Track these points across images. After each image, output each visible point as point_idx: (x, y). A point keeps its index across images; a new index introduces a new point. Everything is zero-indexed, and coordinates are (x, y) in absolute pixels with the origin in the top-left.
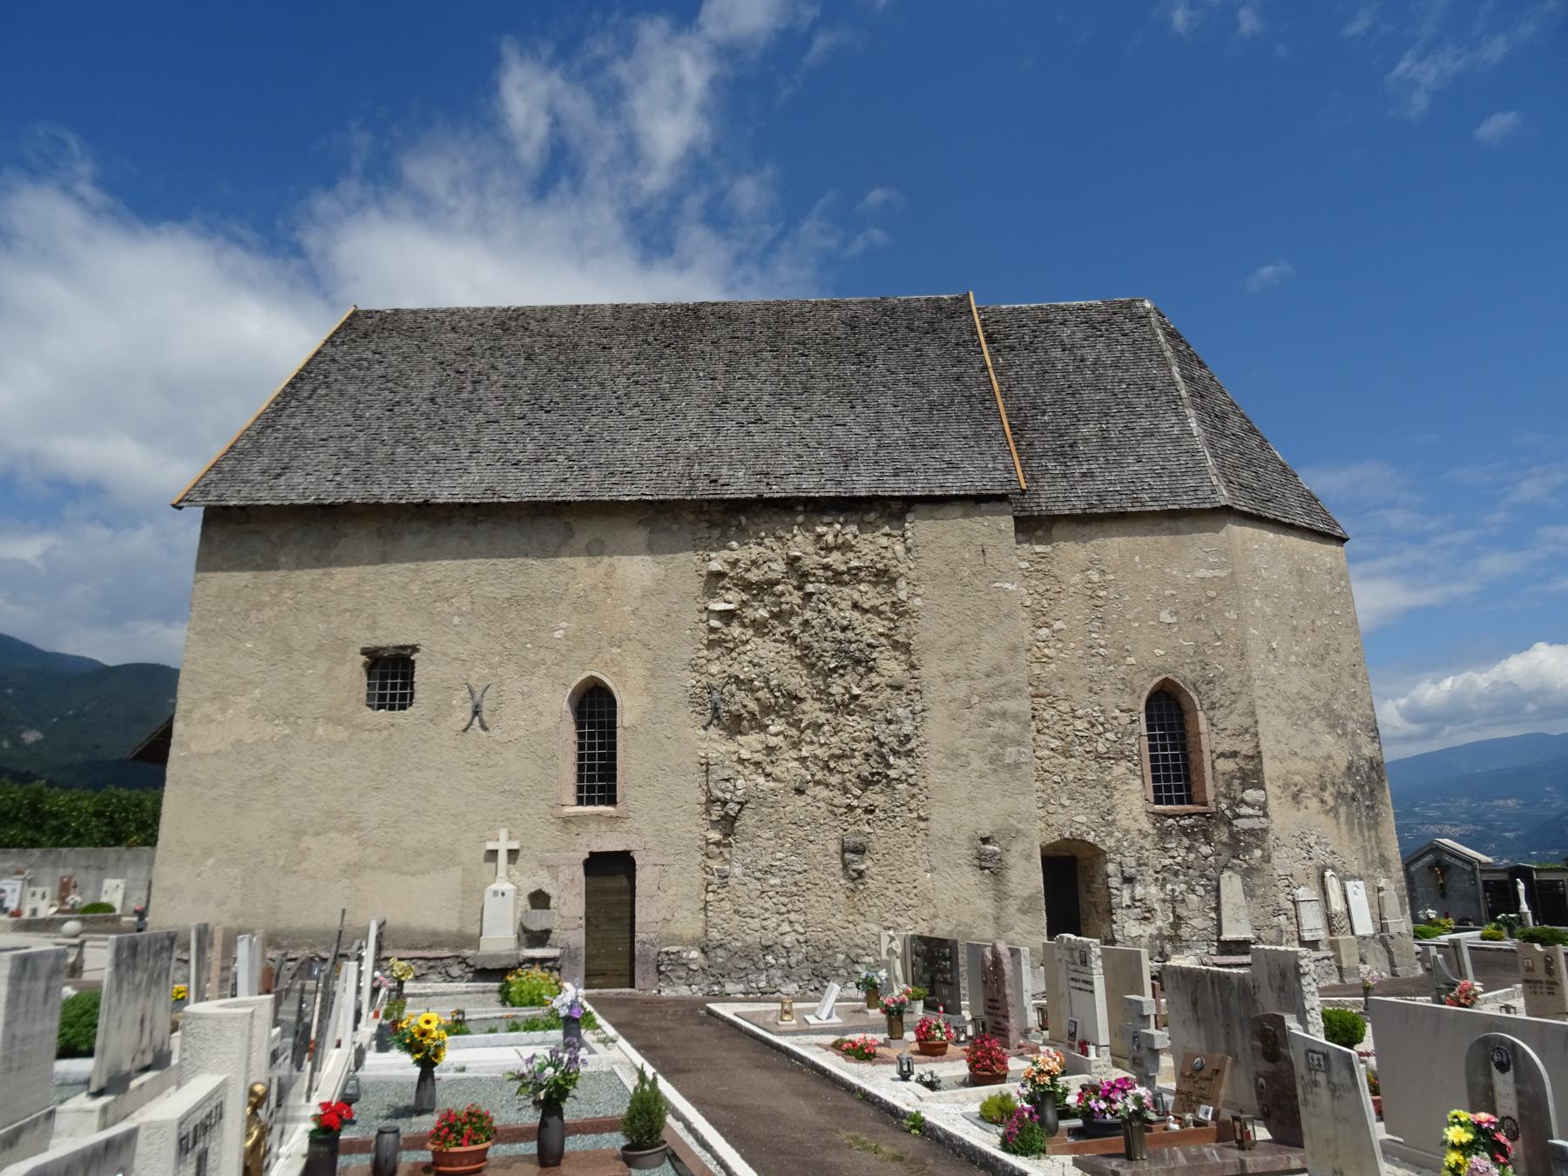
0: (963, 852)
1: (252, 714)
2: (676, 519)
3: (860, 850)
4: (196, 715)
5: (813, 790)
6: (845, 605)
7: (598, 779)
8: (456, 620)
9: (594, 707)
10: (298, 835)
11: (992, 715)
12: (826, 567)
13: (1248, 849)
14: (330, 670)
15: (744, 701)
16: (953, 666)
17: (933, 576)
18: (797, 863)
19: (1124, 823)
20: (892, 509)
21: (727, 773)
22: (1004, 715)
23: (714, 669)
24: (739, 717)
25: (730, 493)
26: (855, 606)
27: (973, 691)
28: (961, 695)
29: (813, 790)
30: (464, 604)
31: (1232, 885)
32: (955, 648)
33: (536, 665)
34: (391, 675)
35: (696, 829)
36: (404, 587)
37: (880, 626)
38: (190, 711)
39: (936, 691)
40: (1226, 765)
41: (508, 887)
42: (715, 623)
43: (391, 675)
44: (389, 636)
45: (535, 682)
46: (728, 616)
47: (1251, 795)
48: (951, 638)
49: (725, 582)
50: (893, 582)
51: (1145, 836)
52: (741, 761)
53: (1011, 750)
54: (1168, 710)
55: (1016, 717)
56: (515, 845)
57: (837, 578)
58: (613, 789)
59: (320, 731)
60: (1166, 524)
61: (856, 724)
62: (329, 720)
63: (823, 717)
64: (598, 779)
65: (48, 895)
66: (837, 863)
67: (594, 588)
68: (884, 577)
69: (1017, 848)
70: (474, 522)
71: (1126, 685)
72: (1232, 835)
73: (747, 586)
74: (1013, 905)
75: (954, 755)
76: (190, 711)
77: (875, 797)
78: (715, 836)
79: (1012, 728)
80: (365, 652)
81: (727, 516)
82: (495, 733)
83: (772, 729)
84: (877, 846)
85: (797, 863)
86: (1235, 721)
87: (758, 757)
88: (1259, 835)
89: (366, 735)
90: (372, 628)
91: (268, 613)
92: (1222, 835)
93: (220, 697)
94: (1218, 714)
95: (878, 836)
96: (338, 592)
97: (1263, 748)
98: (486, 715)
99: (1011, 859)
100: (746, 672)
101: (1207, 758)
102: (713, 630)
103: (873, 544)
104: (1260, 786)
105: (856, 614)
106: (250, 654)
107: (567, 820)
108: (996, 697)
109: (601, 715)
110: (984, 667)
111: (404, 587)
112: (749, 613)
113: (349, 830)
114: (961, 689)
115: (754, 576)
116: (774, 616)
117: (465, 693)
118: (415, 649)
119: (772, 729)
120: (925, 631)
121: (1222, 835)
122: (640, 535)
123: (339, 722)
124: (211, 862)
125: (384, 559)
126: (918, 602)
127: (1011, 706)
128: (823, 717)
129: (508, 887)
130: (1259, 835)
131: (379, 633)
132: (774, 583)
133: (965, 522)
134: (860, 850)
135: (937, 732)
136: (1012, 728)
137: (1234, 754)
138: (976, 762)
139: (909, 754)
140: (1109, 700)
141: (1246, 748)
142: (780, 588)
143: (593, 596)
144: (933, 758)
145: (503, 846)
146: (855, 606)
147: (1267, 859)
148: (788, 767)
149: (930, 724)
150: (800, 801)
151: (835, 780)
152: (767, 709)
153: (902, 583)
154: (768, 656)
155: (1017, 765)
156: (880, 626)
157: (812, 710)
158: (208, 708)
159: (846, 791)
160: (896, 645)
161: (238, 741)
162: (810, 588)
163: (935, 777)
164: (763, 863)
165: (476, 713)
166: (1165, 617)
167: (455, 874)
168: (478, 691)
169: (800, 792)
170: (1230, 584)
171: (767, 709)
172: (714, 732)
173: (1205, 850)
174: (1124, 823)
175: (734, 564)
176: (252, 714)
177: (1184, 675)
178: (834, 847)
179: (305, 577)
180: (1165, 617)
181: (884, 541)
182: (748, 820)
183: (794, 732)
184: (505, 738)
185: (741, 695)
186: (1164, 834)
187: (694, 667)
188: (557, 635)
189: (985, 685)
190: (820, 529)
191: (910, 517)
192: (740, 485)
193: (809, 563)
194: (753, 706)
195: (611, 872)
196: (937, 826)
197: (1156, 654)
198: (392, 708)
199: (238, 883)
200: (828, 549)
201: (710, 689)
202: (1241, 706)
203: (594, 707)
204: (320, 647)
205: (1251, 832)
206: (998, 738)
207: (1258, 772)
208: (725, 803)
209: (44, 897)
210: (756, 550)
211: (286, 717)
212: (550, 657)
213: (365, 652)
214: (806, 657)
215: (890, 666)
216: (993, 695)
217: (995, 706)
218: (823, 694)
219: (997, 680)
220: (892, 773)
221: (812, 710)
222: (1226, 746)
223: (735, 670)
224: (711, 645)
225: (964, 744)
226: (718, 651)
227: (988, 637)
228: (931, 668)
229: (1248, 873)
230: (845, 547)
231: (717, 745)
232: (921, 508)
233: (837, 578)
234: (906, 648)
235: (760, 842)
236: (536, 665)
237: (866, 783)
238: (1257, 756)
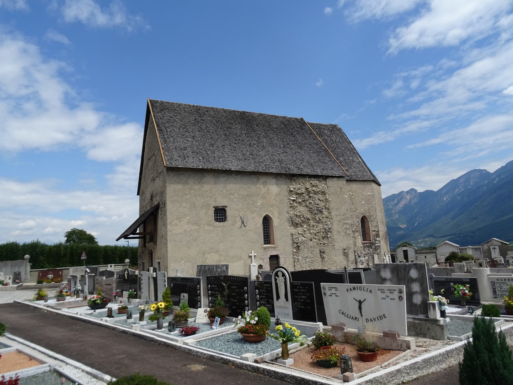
0: (341, 252)
1: (188, 223)
2: (281, 177)
3: (323, 253)
4: (173, 223)
5: (314, 240)
6: (317, 199)
7: (268, 238)
8: (235, 200)
9: (267, 221)
10: (204, 254)
11: (344, 224)
12: (313, 191)
13: (377, 250)
14: (206, 212)
15: (298, 220)
16: (337, 213)
17: (333, 193)
18: (312, 256)
19: (358, 245)
20: (325, 178)
21: (297, 237)
22: (346, 223)
23: (291, 213)
24: (297, 224)
25: (292, 172)
26: (319, 199)
27: (341, 218)
28: (339, 219)
29: (314, 240)
30: (236, 195)
31: (376, 256)
32: (338, 209)
33: (255, 211)
34: (220, 214)
35: (290, 249)
36: (222, 191)
37: (323, 204)
38: (171, 222)
39: (335, 219)
40: (374, 233)
41: (255, 264)
42: (292, 202)
43: (220, 214)
44: (220, 203)
45: (255, 215)
46: (294, 200)
47: (378, 239)
48: (337, 207)
49: (293, 193)
50: (325, 194)
51: (361, 247)
52: (299, 234)
53: (348, 231)
54: (364, 220)
55: (348, 224)
56: (256, 254)
57: (315, 193)
58: (272, 240)
59: (206, 228)
60: (363, 183)
61: (321, 226)
62: (208, 225)
63: (315, 224)
64: (268, 238)
65: (11, 278)
66: (319, 255)
67: (265, 193)
68: (324, 193)
69: (350, 251)
70: (237, 175)
71: (357, 217)
72: (375, 247)
73: (297, 194)
74: (350, 262)
75: (338, 232)
76: (171, 222)
77: (325, 241)
78: (295, 251)
79: (348, 226)
80: (214, 207)
81: (292, 177)
82: (247, 228)
83: (305, 227)
84: (326, 251)
85: (312, 256)
86: (375, 224)
87: (302, 233)
88: (379, 246)
89: (217, 229)
90: (215, 201)
91: (188, 197)
92: (374, 247)
93: (179, 219)
94: (372, 222)
95: (326, 249)
96: (206, 191)
97: (380, 230)
98: (245, 223)
99: (350, 253)
100: (298, 214)
101: (371, 231)
102: (291, 204)
103: (321, 185)
104: (379, 237)
105: (319, 201)
106: (185, 207)
107: (265, 248)
108: (345, 220)
109: (266, 223)
110: (343, 214)
111: (222, 191)
112: (298, 200)
113: (216, 252)
114: (339, 218)
115: (299, 192)
116: (303, 201)
117: (239, 218)
118: (226, 207)
119: (305, 227)
120: (332, 205)
121: (374, 247)
122: (274, 181)
123: (210, 225)
124: (183, 262)
125: (216, 183)
126: (330, 199)
127: (348, 222)
128: (315, 224)
129: (255, 264)
130: (379, 246)
131: (217, 202)
132: (303, 194)
133: (338, 182)
134: (323, 253)
135: (335, 227)
136: (348, 226)
137: (375, 231)
138: (343, 234)
139: (330, 232)
140: (354, 220)
141: (377, 230)
142: (304, 195)
143: (265, 195)
144: (335, 233)
145: (253, 255)
146: (319, 199)
147: (380, 251)
148: (308, 235)
149: (334, 225)
150: (311, 242)
151: (317, 237)
152: (303, 222)
153: (327, 195)
154: (302, 210)
155: (349, 234)
156: (323, 204)
157: (312, 222)
158: (176, 221)
159: (319, 240)
160: (326, 208)
161: (185, 230)
162: (311, 195)
163: (335, 237)
164: (305, 256)
165: (243, 223)
166: (363, 203)
167: (242, 262)
168: (242, 217)
169: (311, 240)
170: (373, 196)
171: (303, 222)
172: (292, 227)
173: (371, 250)
174: (358, 245)
175: (294, 189)
176: (188, 223)
177: (367, 215)
178: (318, 252)
179: (197, 187)
180: (363, 203)
181: (323, 185)
182: (302, 247)
183: (308, 227)
184: (250, 229)
185: (297, 219)
186: (364, 247)
187: (288, 213)
188: (259, 204)
189: (343, 217)
190: (312, 182)
191: (328, 180)
192: (295, 171)
193: (310, 189)
194: (300, 221)
195: (274, 259)
196: (337, 246)
197: (361, 211)
198: (220, 222)
199: (191, 267)
200: (313, 186)
201: (291, 217)
202: (376, 221)
203: (267, 221)
204: (203, 206)
205: (378, 246)
206: (346, 228)
207: (379, 234)
208: (297, 243)
209: (10, 279)
210: (299, 186)
211: (197, 224)
212: (258, 210)
213: (214, 207)
214: (311, 211)
215: (325, 213)
216: (344, 219)
217: (345, 222)
218: (314, 219)
219: (345, 216)
220: (328, 236)
221: (312, 222)
222: (373, 230)
223: (296, 213)
224: (291, 207)
225: (340, 229)
226: (292, 209)
227: (343, 207)
228: (333, 213)
229: (378, 254)
230: (316, 186)
231: (292, 230)
232: (330, 178)
233: (315, 193)
234: (328, 209)
235: (305, 252)
236: (255, 211)
237: (323, 238)
238: (378, 231)
